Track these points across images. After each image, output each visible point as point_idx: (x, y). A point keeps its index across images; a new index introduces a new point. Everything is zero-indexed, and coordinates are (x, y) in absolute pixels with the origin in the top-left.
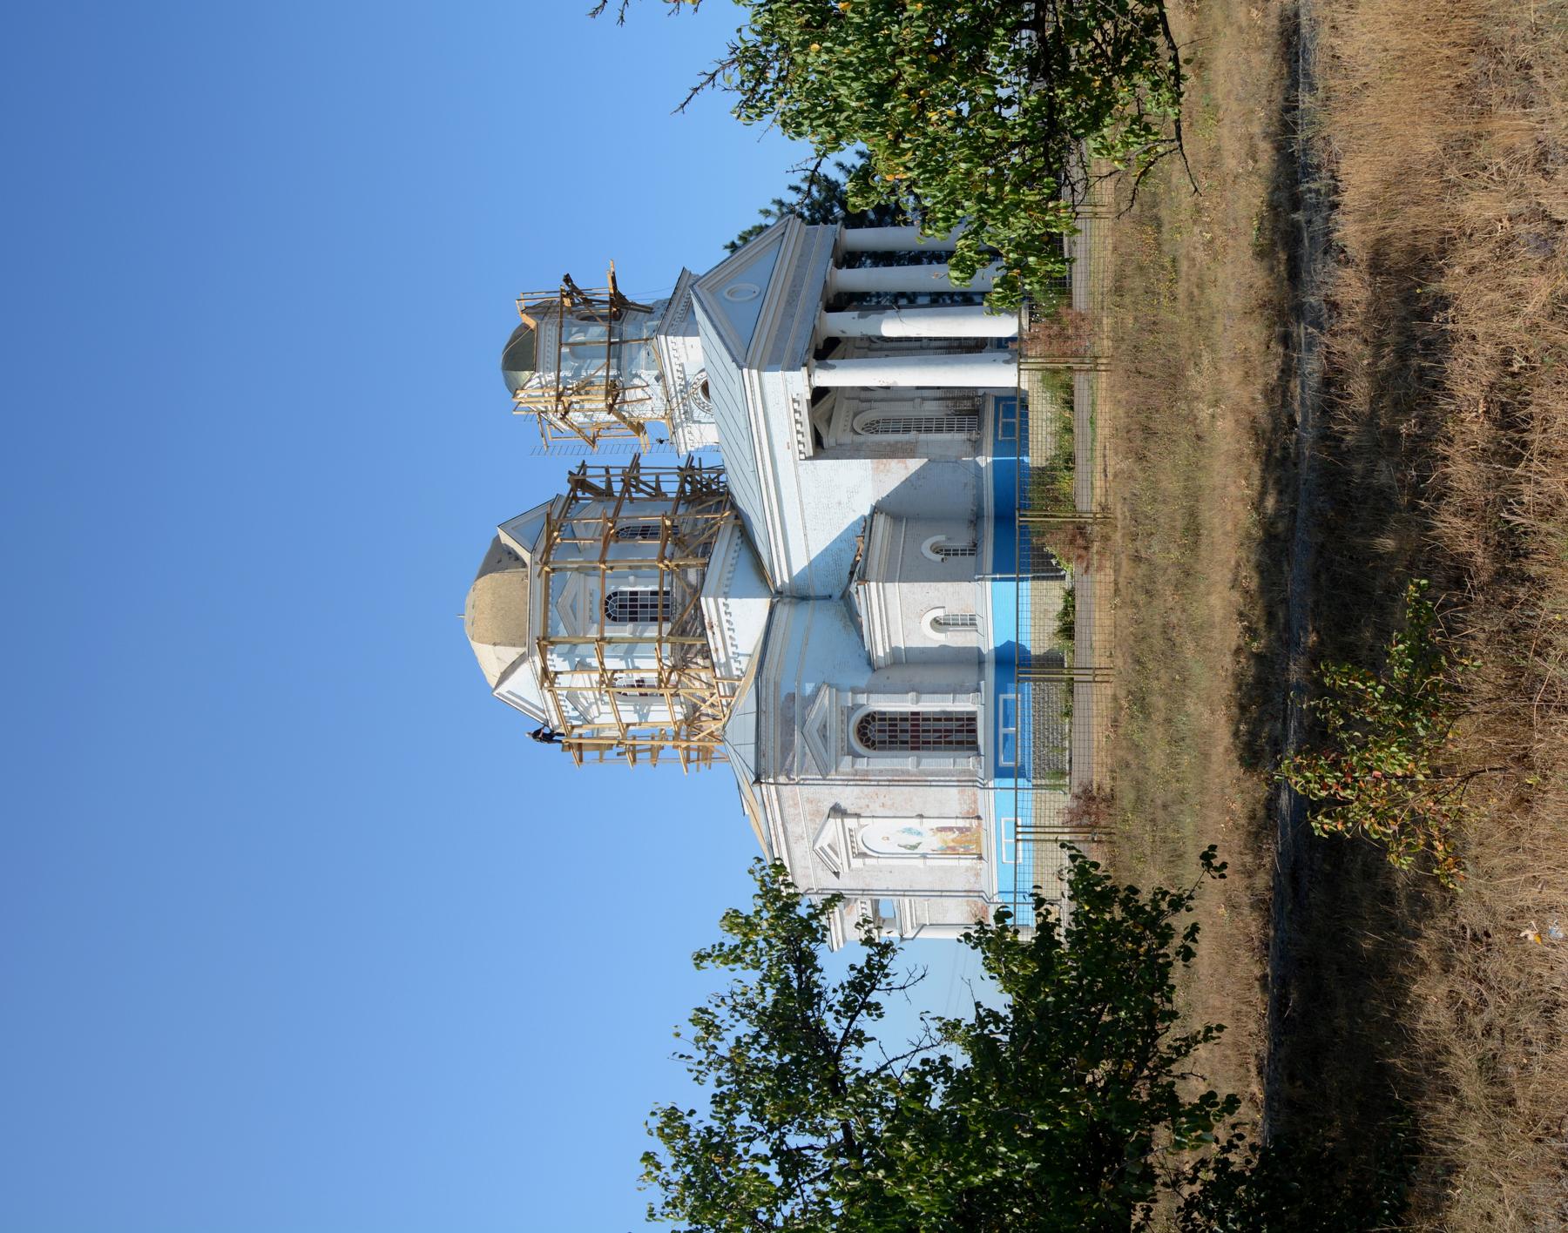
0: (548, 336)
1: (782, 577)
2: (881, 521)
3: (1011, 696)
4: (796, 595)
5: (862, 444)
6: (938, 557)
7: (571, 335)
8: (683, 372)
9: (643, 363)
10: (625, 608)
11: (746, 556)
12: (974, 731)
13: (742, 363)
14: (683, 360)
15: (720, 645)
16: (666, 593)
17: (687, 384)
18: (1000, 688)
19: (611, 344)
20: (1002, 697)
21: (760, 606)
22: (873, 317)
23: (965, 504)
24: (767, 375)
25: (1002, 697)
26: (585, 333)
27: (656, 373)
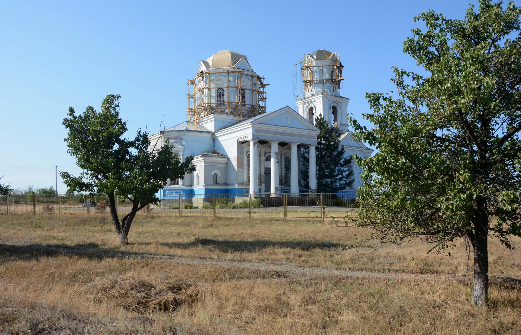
0: (326, 62)
1: (217, 134)
2: (224, 160)
3: (182, 193)
4: (214, 139)
5: (243, 154)
6: (213, 174)
7: (326, 69)
8: (315, 101)
9: (318, 90)
10: (220, 93)
11: (230, 124)
12: (175, 185)
13: (253, 122)
14: (317, 101)
15: (210, 118)
16: (224, 104)
17: (312, 103)
18: (184, 191)
19: (323, 80)
20: (182, 191)
21: (212, 129)
22: (275, 156)
23: (230, 182)
24: (251, 129)
25: (182, 191)
26: (327, 73)
27: (315, 94)
